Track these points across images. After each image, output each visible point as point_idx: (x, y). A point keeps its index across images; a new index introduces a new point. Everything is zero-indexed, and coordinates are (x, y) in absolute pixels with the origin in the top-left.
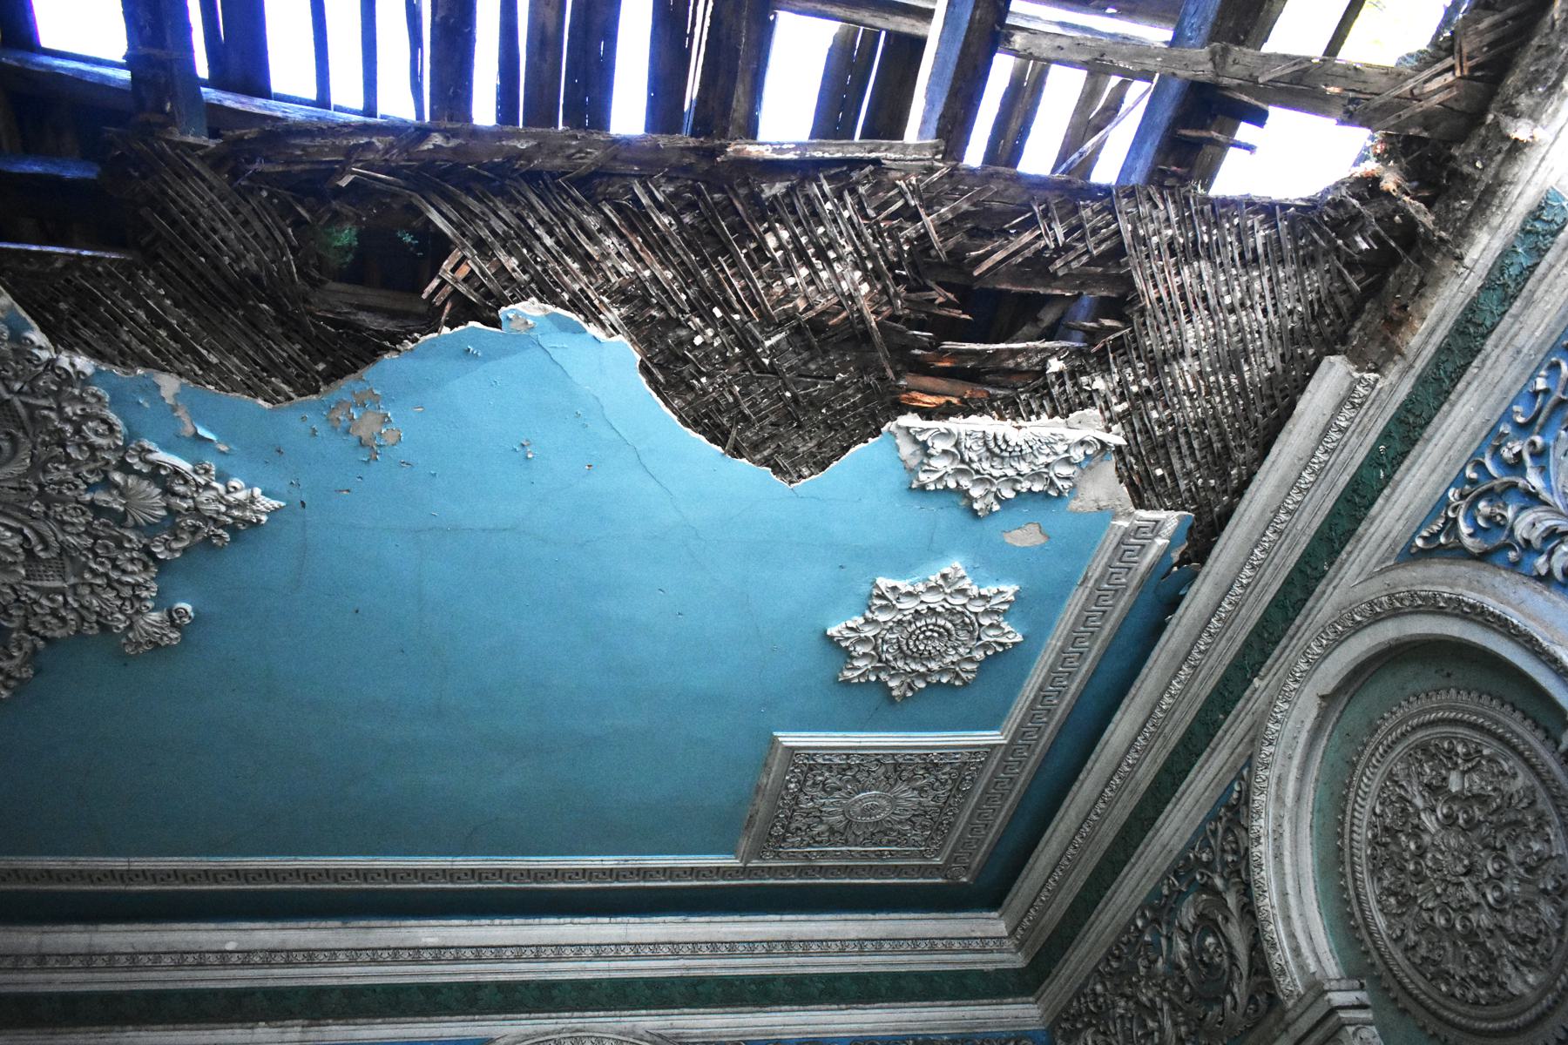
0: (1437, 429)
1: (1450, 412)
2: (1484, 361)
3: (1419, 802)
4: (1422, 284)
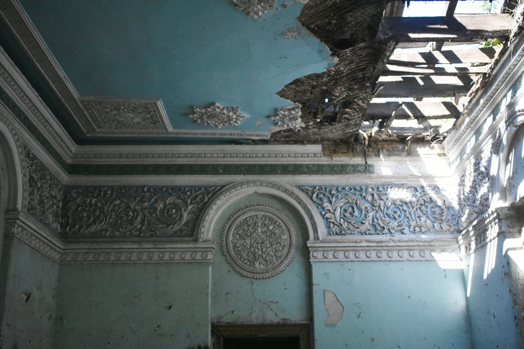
3: (260, 225)
4: (345, 153)
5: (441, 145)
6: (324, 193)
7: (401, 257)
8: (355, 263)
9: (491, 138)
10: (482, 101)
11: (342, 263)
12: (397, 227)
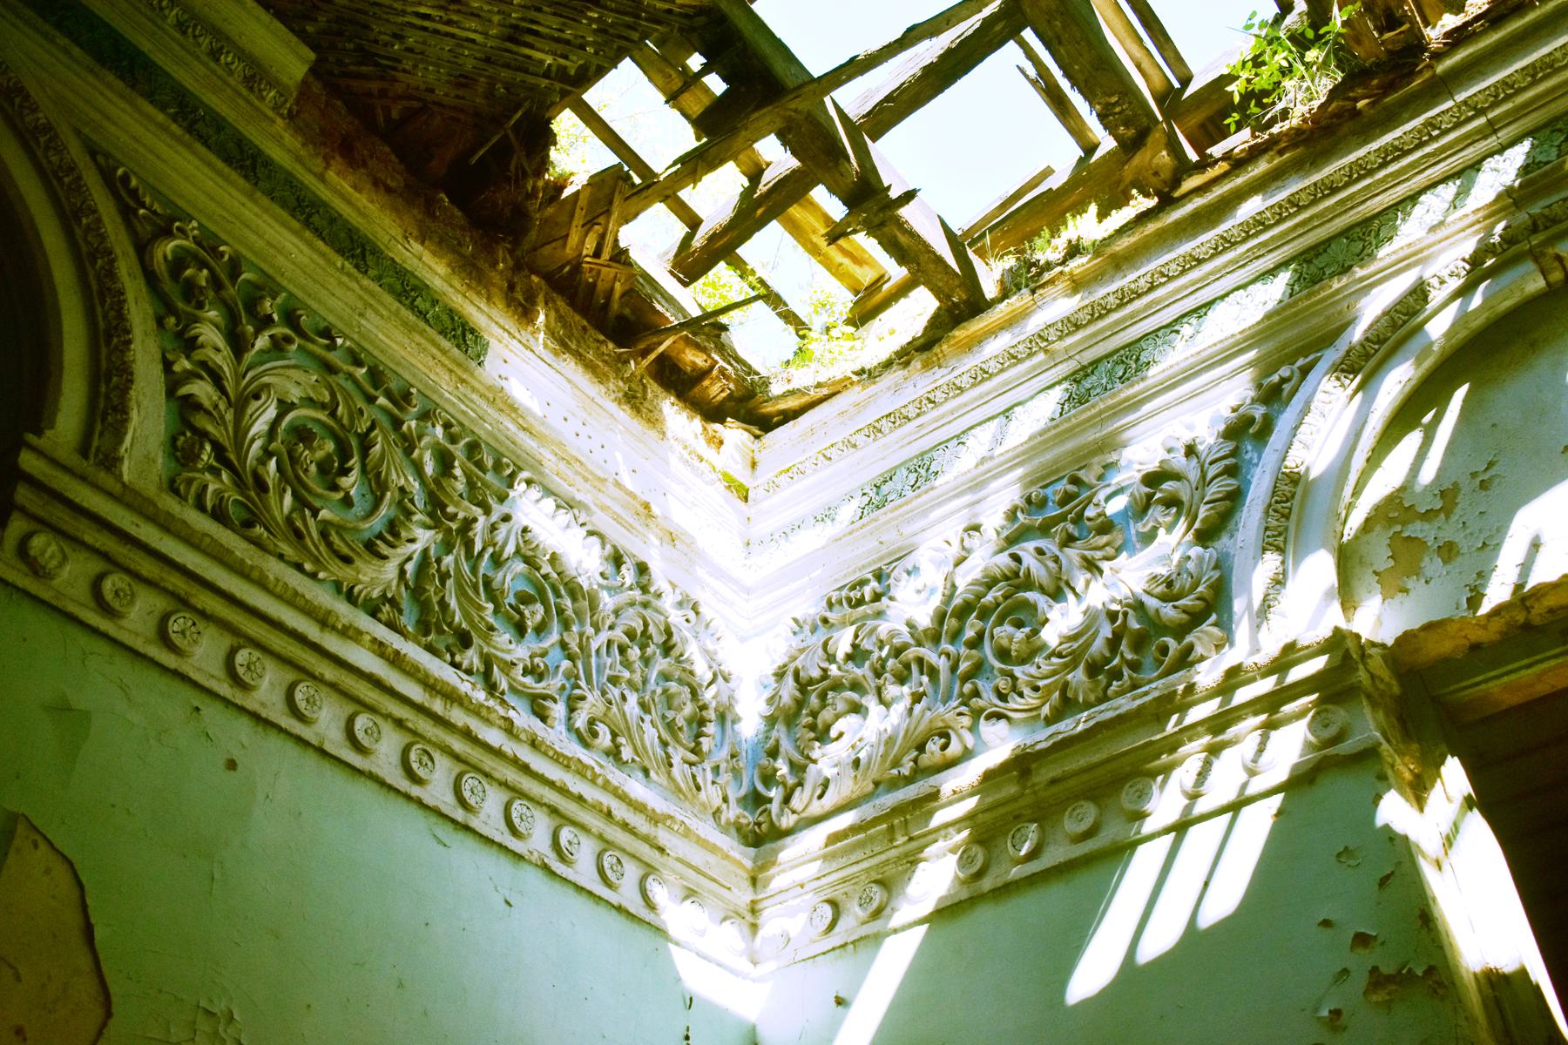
0: (266, 210)
1: (290, 229)
2: (349, 275)
4: (389, 190)
5: (757, 445)
6: (223, 277)
7: (514, 831)
8: (273, 734)
9: (1020, 479)
10: (1252, 206)
11: (197, 699)
12: (526, 672)
